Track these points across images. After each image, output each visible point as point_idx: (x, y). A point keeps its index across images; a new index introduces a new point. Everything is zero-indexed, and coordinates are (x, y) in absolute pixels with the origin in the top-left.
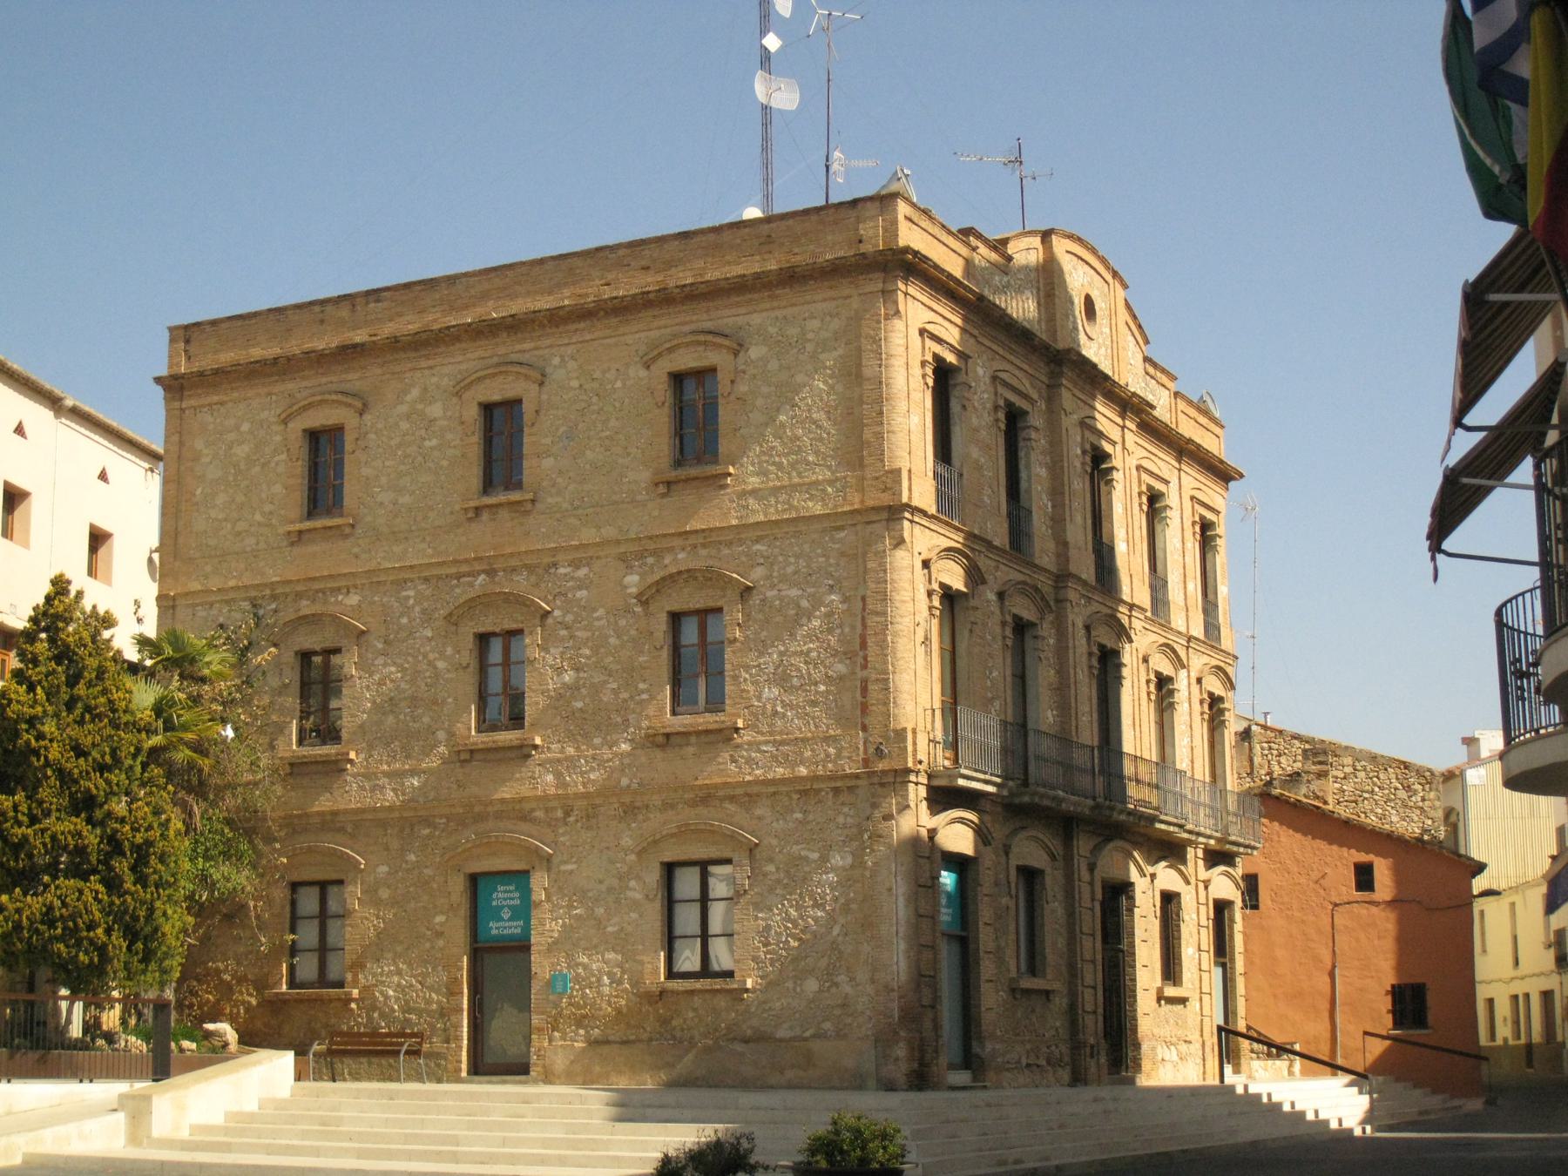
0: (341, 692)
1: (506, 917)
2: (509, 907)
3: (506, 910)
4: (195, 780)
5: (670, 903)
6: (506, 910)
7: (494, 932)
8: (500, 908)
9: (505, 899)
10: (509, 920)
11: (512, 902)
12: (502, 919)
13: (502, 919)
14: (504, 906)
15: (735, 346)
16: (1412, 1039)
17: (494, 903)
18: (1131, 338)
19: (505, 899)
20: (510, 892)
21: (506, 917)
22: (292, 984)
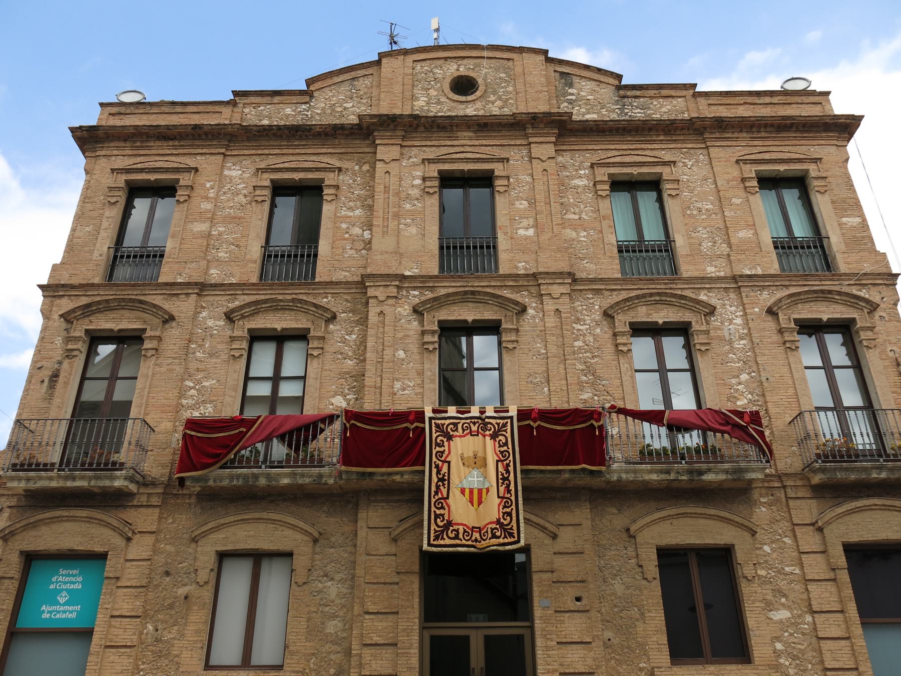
0: (176, 191)
1: (62, 600)
2: (66, 590)
3: (64, 594)
4: (198, 310)
5: (869, 407)
6: (64, 594)
7: (45, 616)
8: (59, 592)
9: (65, 583)
10: (65, 604)
11: (72, 587)
12: (58, 603)
13: (58, 603)
14: (63, 590)
15: (316, 534)
16: (632, 291)
17: (52, 587)
18: (273, 453)
19: (65, 583)
20: (73, 576)
21: (62, 600)
22: (429, 545)
